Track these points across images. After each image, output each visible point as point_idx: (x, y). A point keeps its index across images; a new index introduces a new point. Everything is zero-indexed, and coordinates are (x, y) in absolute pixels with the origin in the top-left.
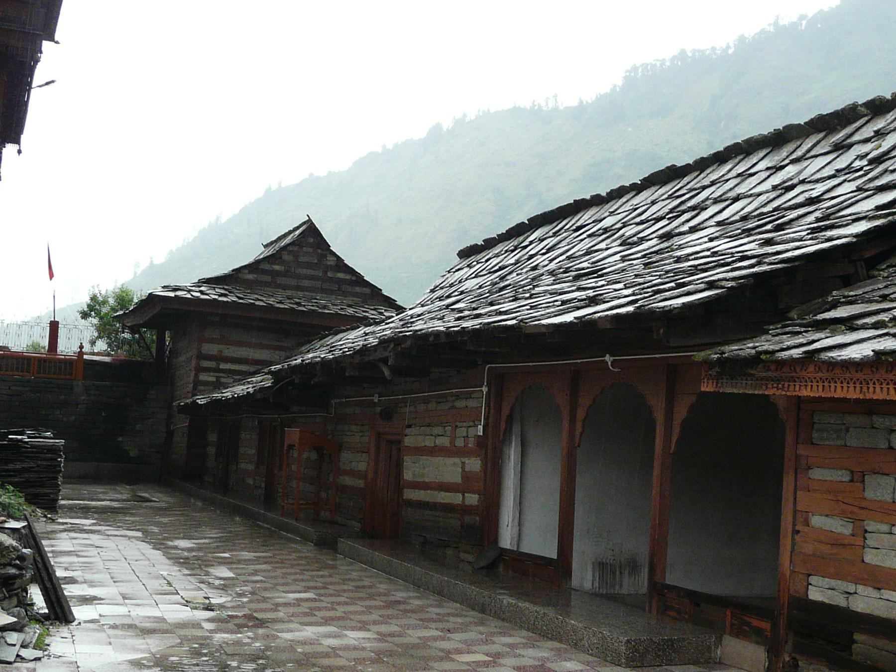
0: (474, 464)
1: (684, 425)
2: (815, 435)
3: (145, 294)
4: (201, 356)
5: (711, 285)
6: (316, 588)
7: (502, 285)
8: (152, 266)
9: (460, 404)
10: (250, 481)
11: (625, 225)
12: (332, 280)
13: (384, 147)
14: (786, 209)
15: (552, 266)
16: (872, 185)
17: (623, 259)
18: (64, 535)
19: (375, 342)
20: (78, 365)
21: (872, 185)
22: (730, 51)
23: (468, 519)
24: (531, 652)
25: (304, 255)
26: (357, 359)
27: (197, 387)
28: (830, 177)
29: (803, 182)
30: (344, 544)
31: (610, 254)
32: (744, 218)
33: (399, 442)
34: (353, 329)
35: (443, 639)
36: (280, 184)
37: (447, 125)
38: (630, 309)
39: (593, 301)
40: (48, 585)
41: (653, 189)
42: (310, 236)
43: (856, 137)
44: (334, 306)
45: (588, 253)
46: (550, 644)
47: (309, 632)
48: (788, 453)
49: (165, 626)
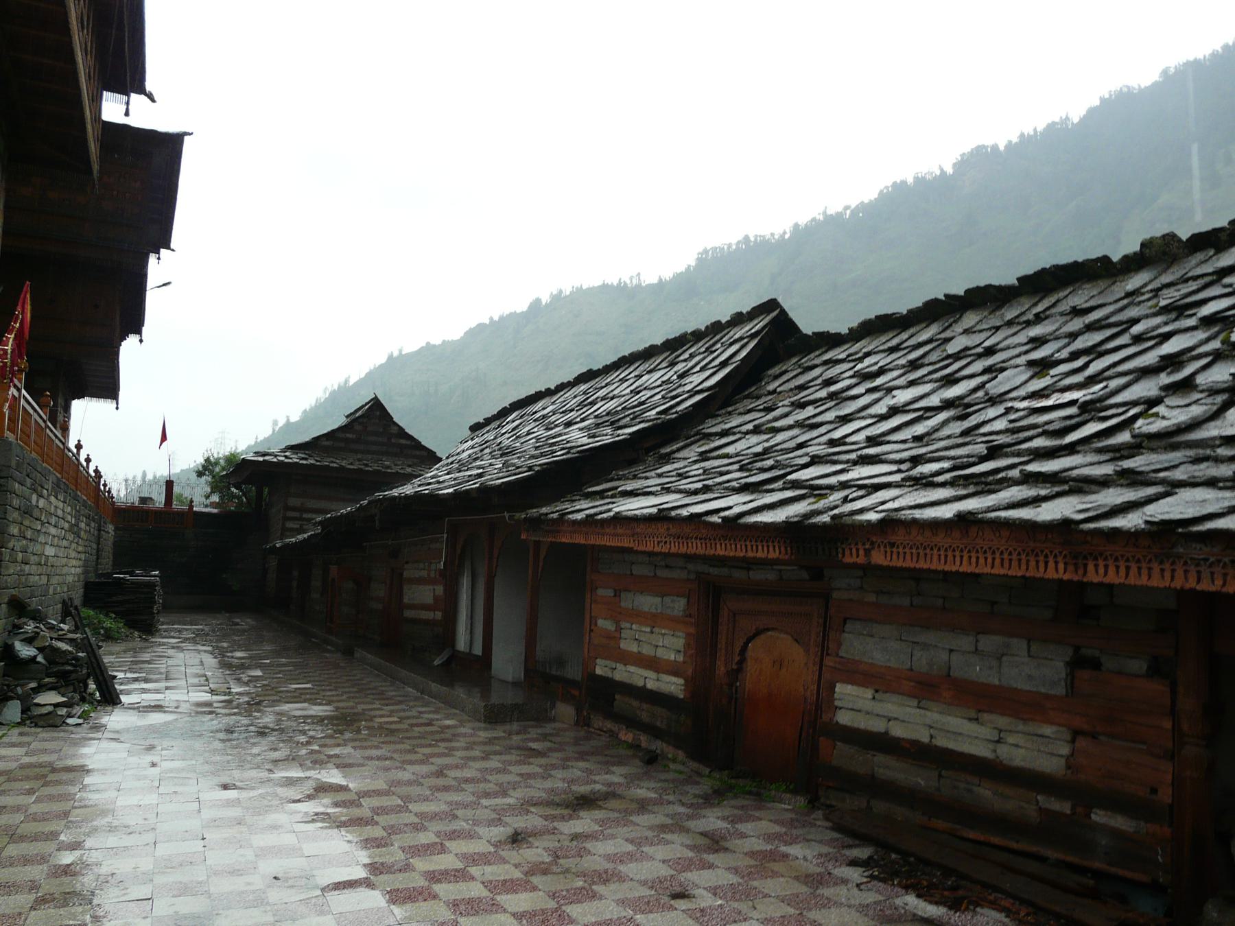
4: (287, 508)
13: (491, 319)
20: (191, 517)
22: (787, 236)
27: (285, 532)
30: (359, 653)
33: (401, 575)
36: (400, 351)
37: (545, 299)
38: (451, 490)
44: (391, 465)
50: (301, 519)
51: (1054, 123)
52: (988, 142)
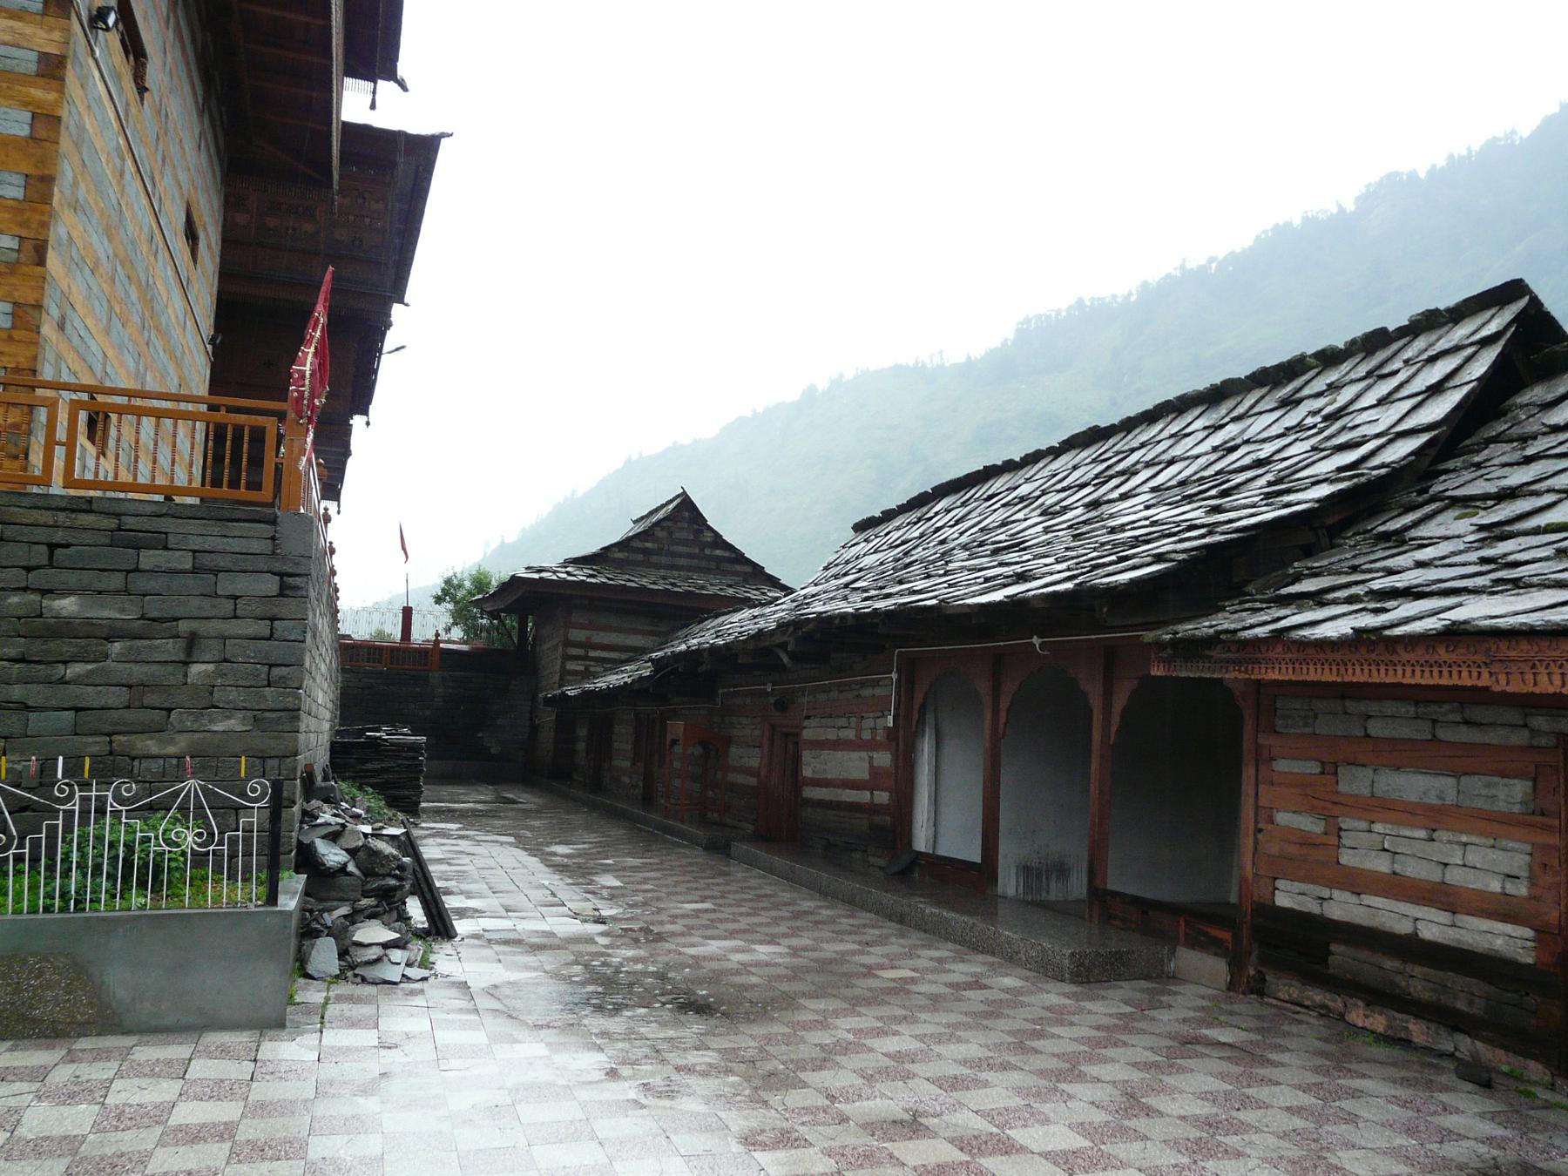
0: (884, 759)
1: (1125, 711)
2: (1279, 722)
3: (505, 576)
4: (568, 643)
5: (1159, 558)
6: (712, 897)
7: (907, 560)
8: (503, 545)
9: (867, 692)
10: (626, 780)
11: (1044, 493)
12: (710, 558)
13: (754, 411)
14: (1231, 472)
15: (964, 539)
16: (1329, 444)
17: (1046, 530)
18: (430, 841)
19: (773, 626)
20: (433, 654)
21: (1329, 444)
22: (1133, 299)
23: (878, 819)
24: (961, 967)
25: (679, 530)
26: (751, 646)
27: (565, 677)
28: (1278, 436)
29: (1247, 442)
30: (738, 847)
31: (1031, 525)
32: (1182, 484)
33: (797, 735)
34: (736, 611)
35: (861, 953)
37: (822, 386)
38: (1069, 585)
39: (1022, 577)
40: (428, 897)
41: (1074, 453)
42: (685, 511)
43: (1306, 392)
44: (713, 587)
45: (1003, 524)
46: (981, 958)
47: (714, 947)
48: (1247, 742)
49: (556, 941)
50: (586, 658)
51: (1495, 139)
52: (1404, 167)
